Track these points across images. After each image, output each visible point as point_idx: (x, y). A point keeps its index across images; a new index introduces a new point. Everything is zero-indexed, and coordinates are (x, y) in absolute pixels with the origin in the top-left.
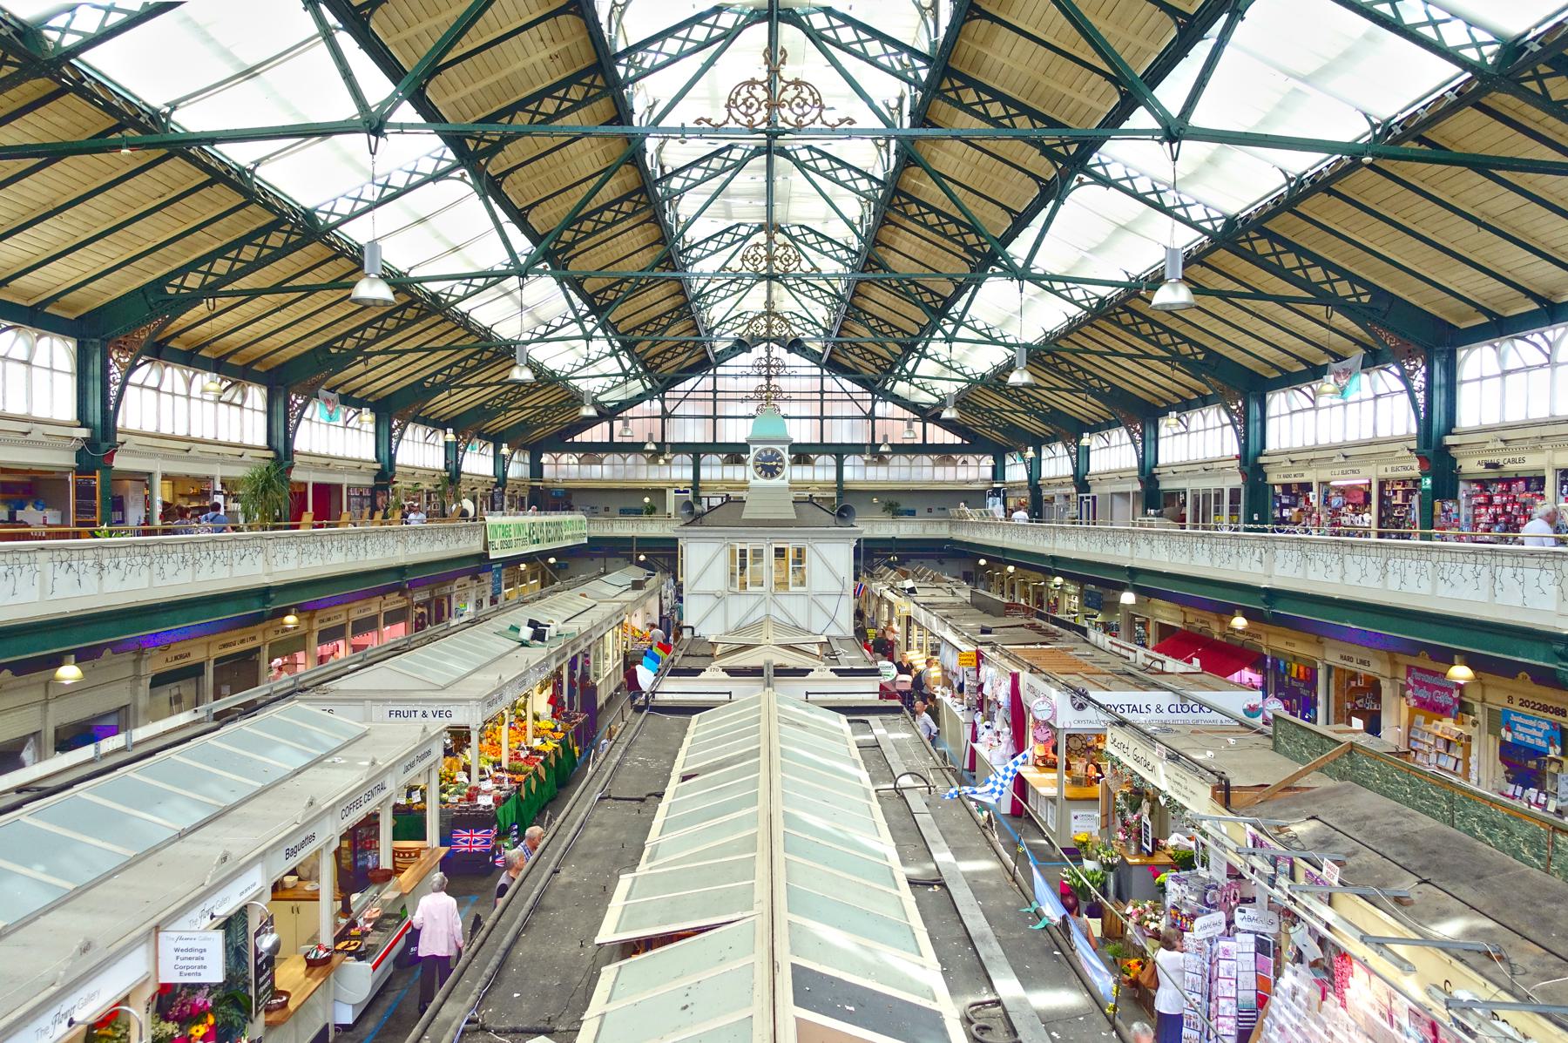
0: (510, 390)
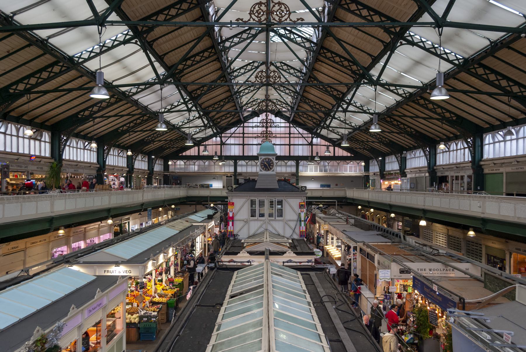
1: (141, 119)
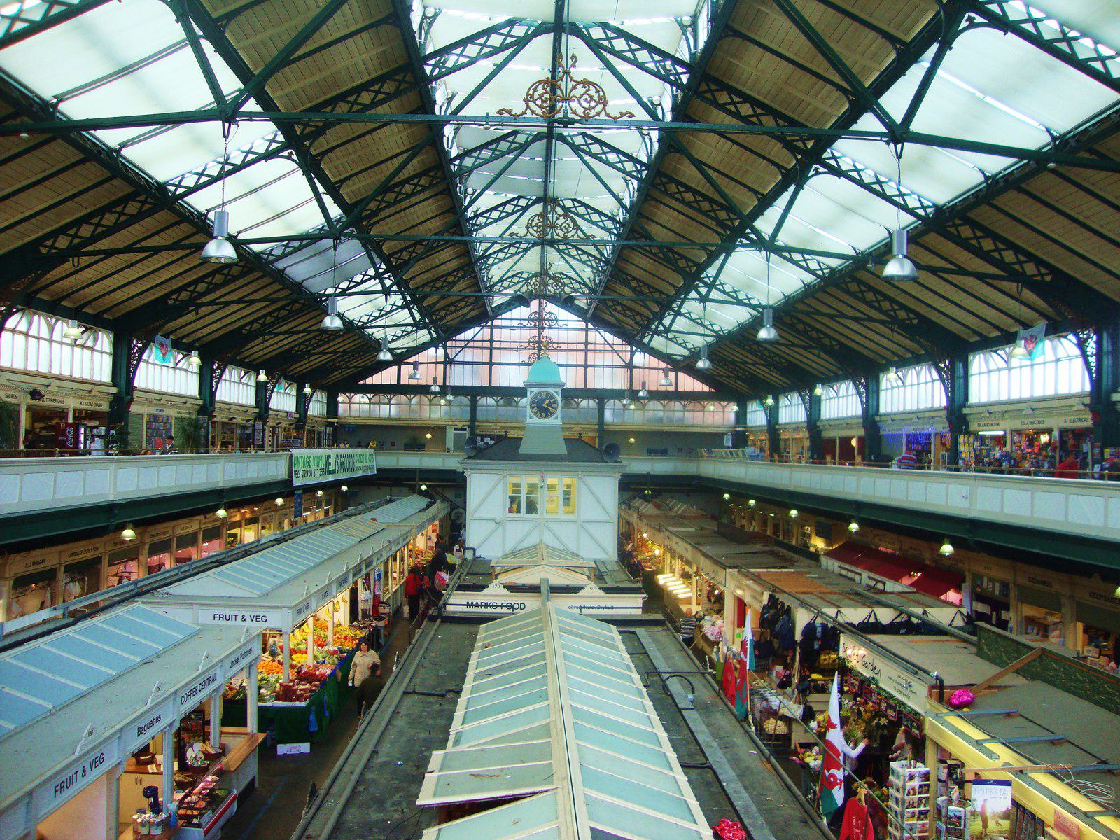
0: (314, 338)
1: (289, 308)
